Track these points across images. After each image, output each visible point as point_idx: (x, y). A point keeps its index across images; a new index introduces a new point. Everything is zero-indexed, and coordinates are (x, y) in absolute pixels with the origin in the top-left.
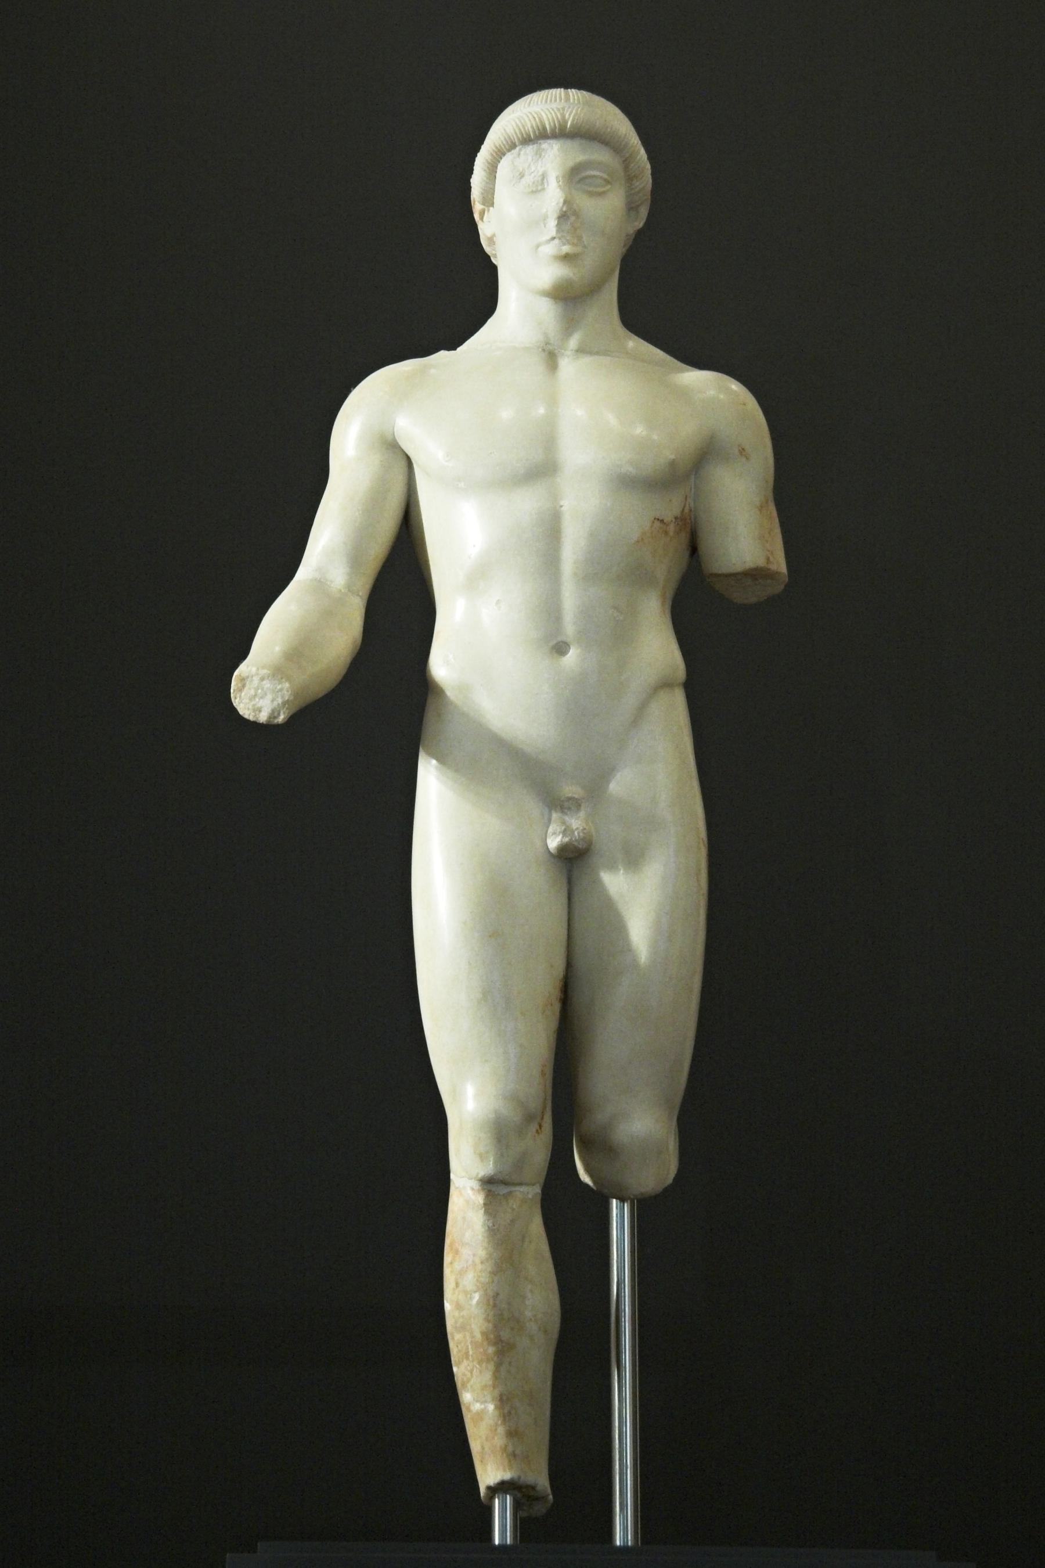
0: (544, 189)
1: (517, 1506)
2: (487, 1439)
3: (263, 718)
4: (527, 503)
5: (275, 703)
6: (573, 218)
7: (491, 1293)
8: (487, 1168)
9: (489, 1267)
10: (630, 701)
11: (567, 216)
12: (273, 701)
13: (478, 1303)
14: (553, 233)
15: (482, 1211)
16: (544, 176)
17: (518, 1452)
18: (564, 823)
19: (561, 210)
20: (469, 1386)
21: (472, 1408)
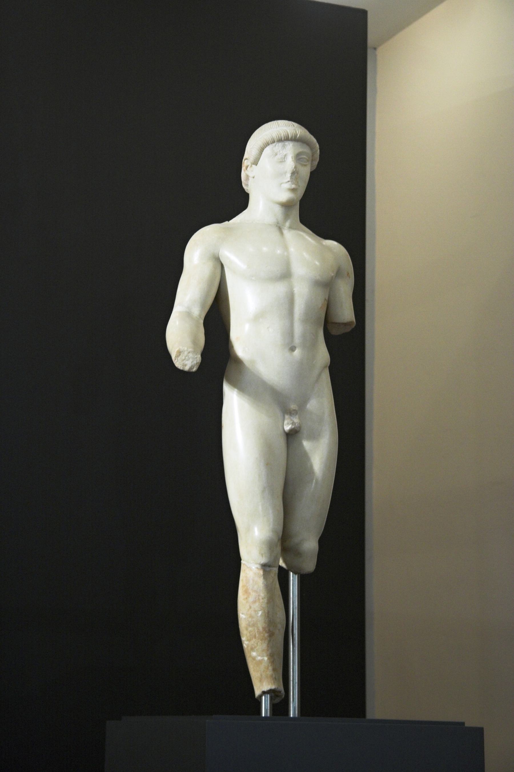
1: (271, 699)
2: (263, 672)
3: (187, 368)
6: (296, 174)
7: (266, 611)
8: (263, 560)
9: (266, 600)
10: (316, 372)
15: (262, 578)
17: (277, 677)
18: (291, 420)
20: (255, 649)
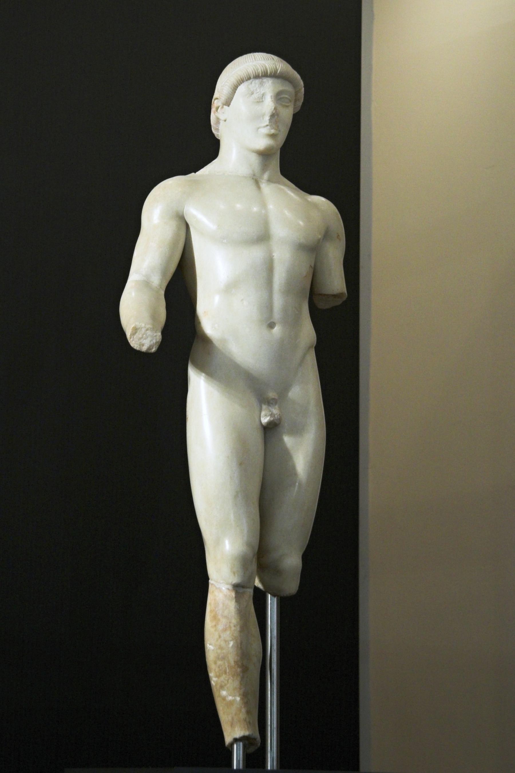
0: (263, 101)
1: (244, 747)
2: (235, 715)
3: (144, 349)
4: (257, 253)
5: (152, 342)
8: (236, 580)
9: (238, 628)
10: (299, 353)
11: (274, 116)
12: (150, 341)
13: (233, 645)
14: (267, 123)
15: (234, 601)
16: (263, 95)
17: (251, 722)
19: (272, 112)
21: (227, 699)
